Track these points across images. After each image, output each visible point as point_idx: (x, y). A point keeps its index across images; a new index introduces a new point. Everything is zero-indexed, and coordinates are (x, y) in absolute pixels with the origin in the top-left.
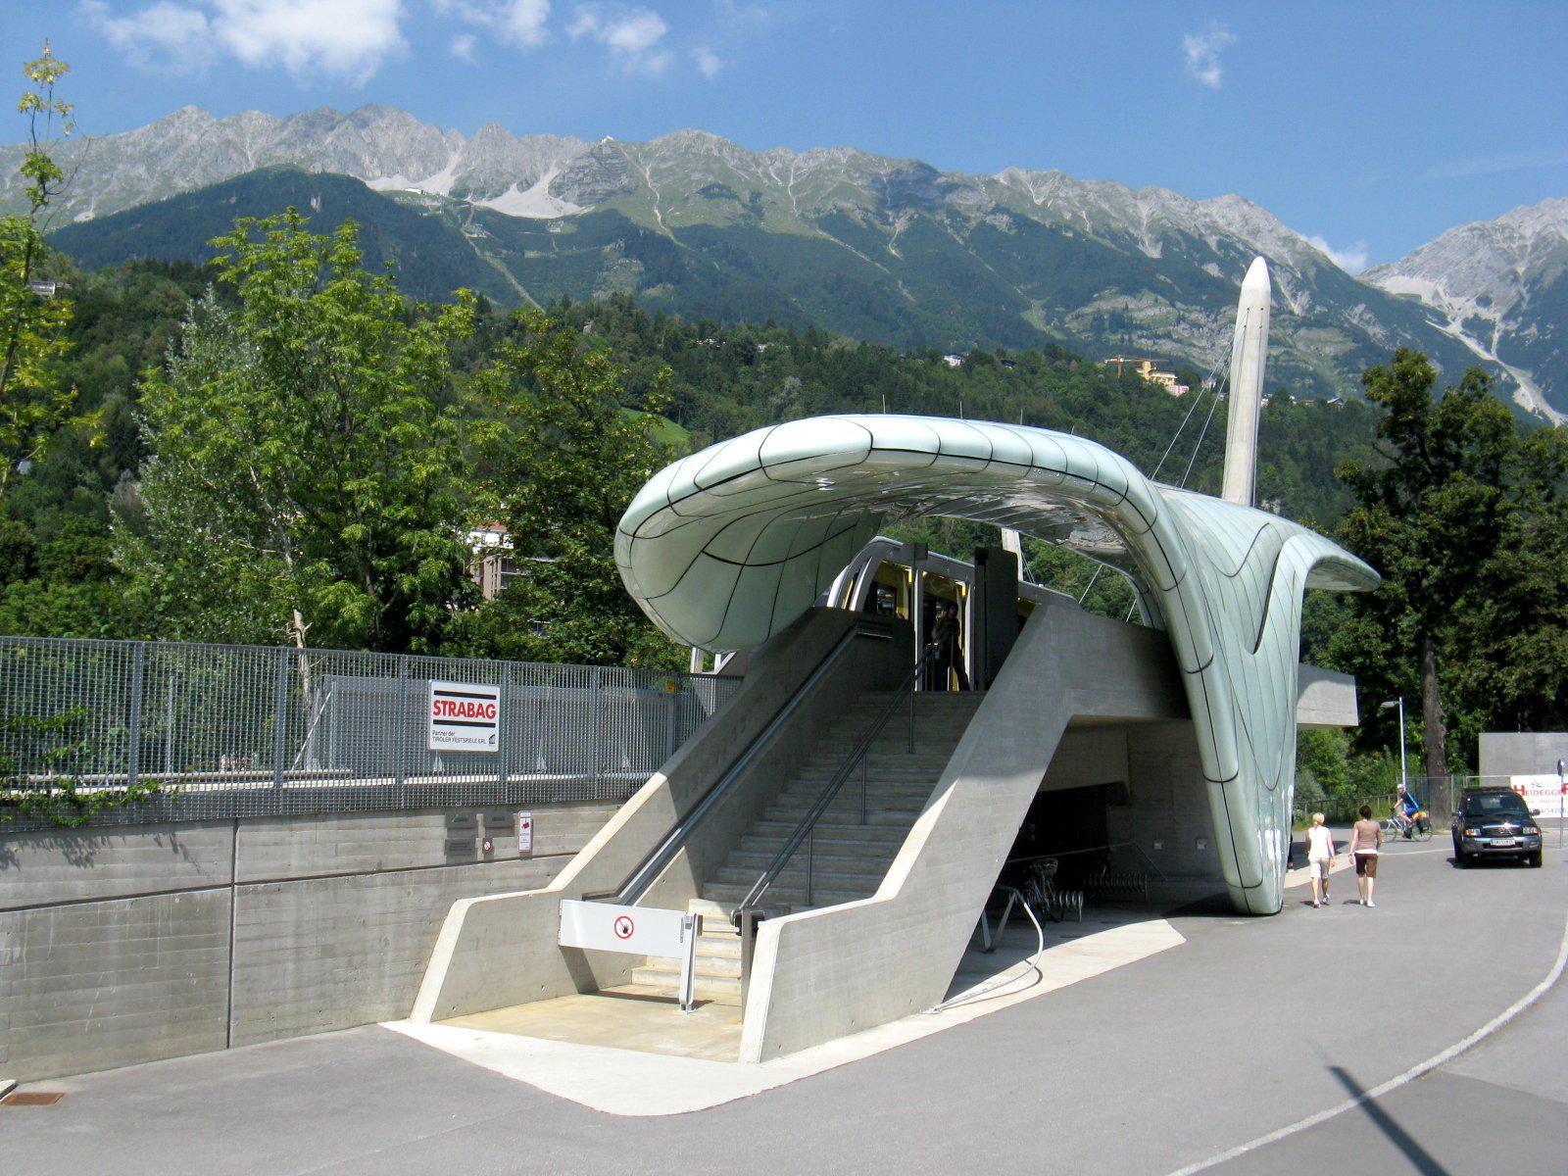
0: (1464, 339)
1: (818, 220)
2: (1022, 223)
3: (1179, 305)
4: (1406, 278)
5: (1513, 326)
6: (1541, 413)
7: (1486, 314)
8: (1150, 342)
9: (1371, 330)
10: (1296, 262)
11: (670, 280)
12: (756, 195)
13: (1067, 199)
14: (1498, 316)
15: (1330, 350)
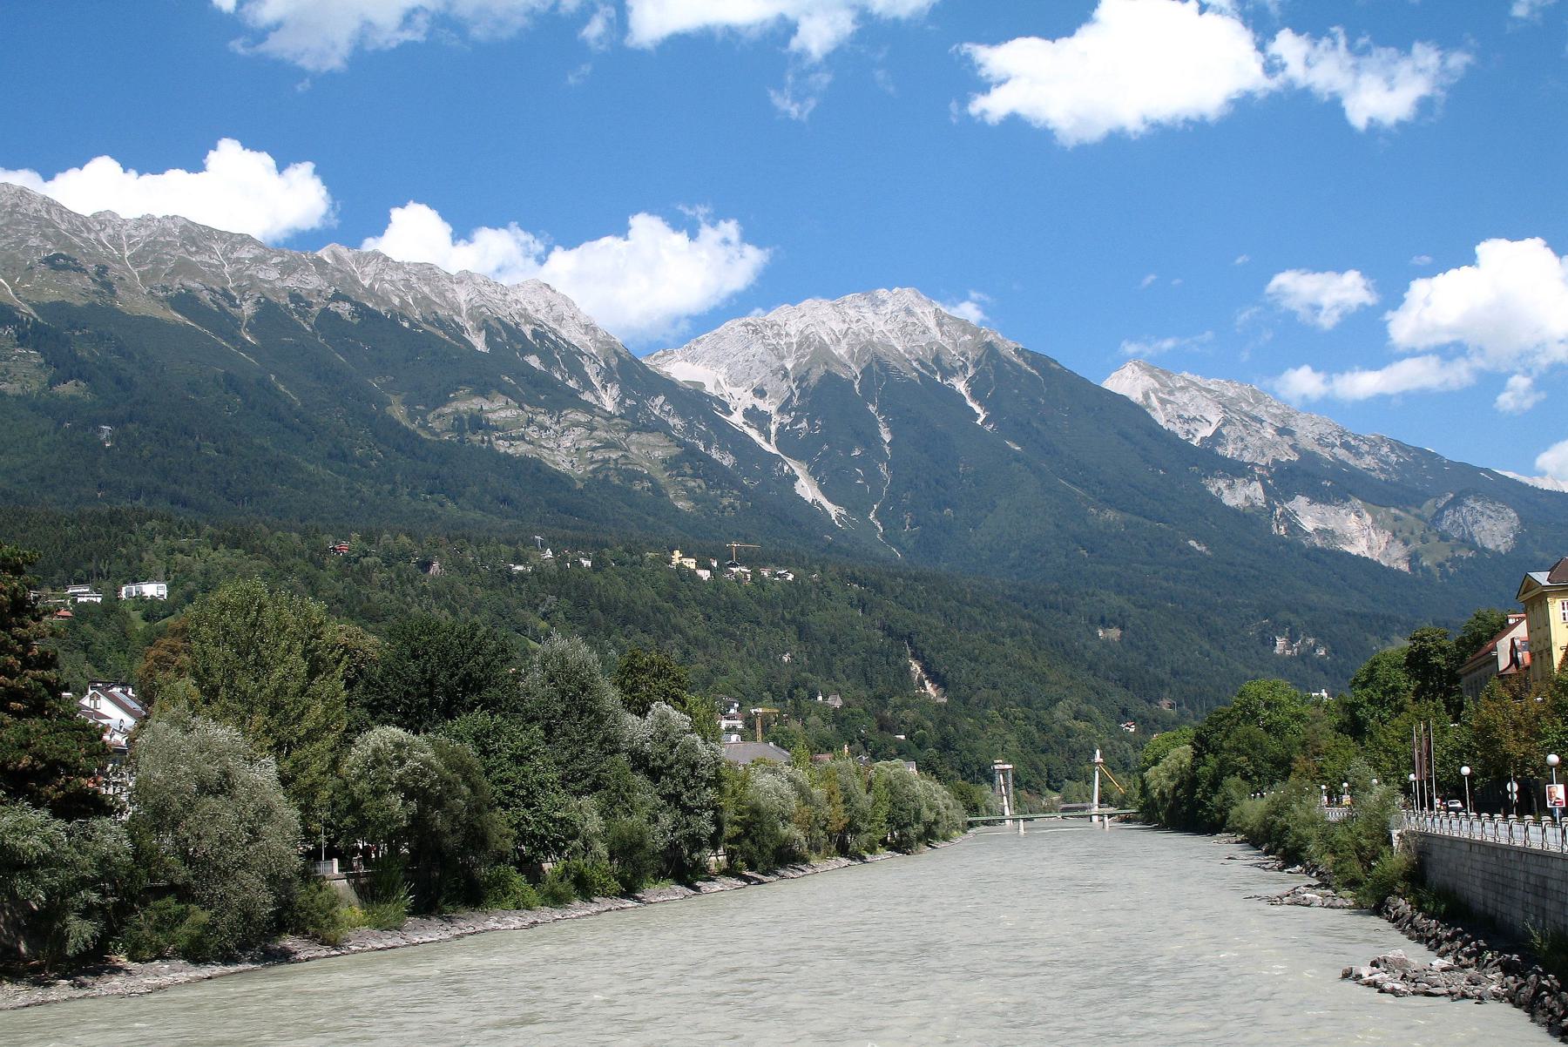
0: (746, 428)
1: (168, 299)
2: (361, 310)
3: (527, 407)
4: (689, 365)
5: (787, 420)
6: (819, 504)
7: (764, 405)
8: (507, 444)
9: (671, 421)
10: (600, 350)
11: (80, 377)
12: (102, 270)
13: (392, 282)
14: (773, 409)
15: (658, 454)
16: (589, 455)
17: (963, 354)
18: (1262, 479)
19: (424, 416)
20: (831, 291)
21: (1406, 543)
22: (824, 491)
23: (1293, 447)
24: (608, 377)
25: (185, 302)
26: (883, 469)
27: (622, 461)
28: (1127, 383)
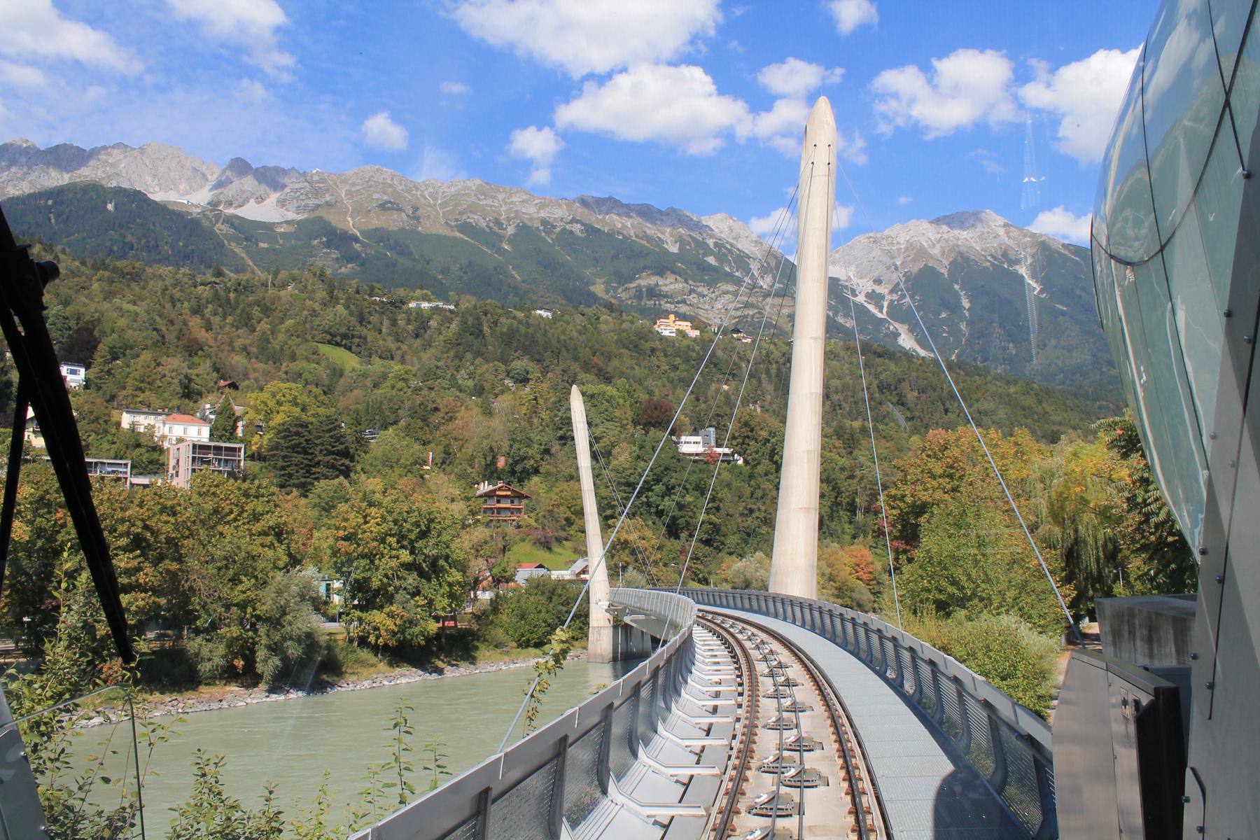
1: (457, 226)
5: (895, 297)
7: (879, 289)
24: (764, 270)
25: (466, 228)
26: (963, 326)
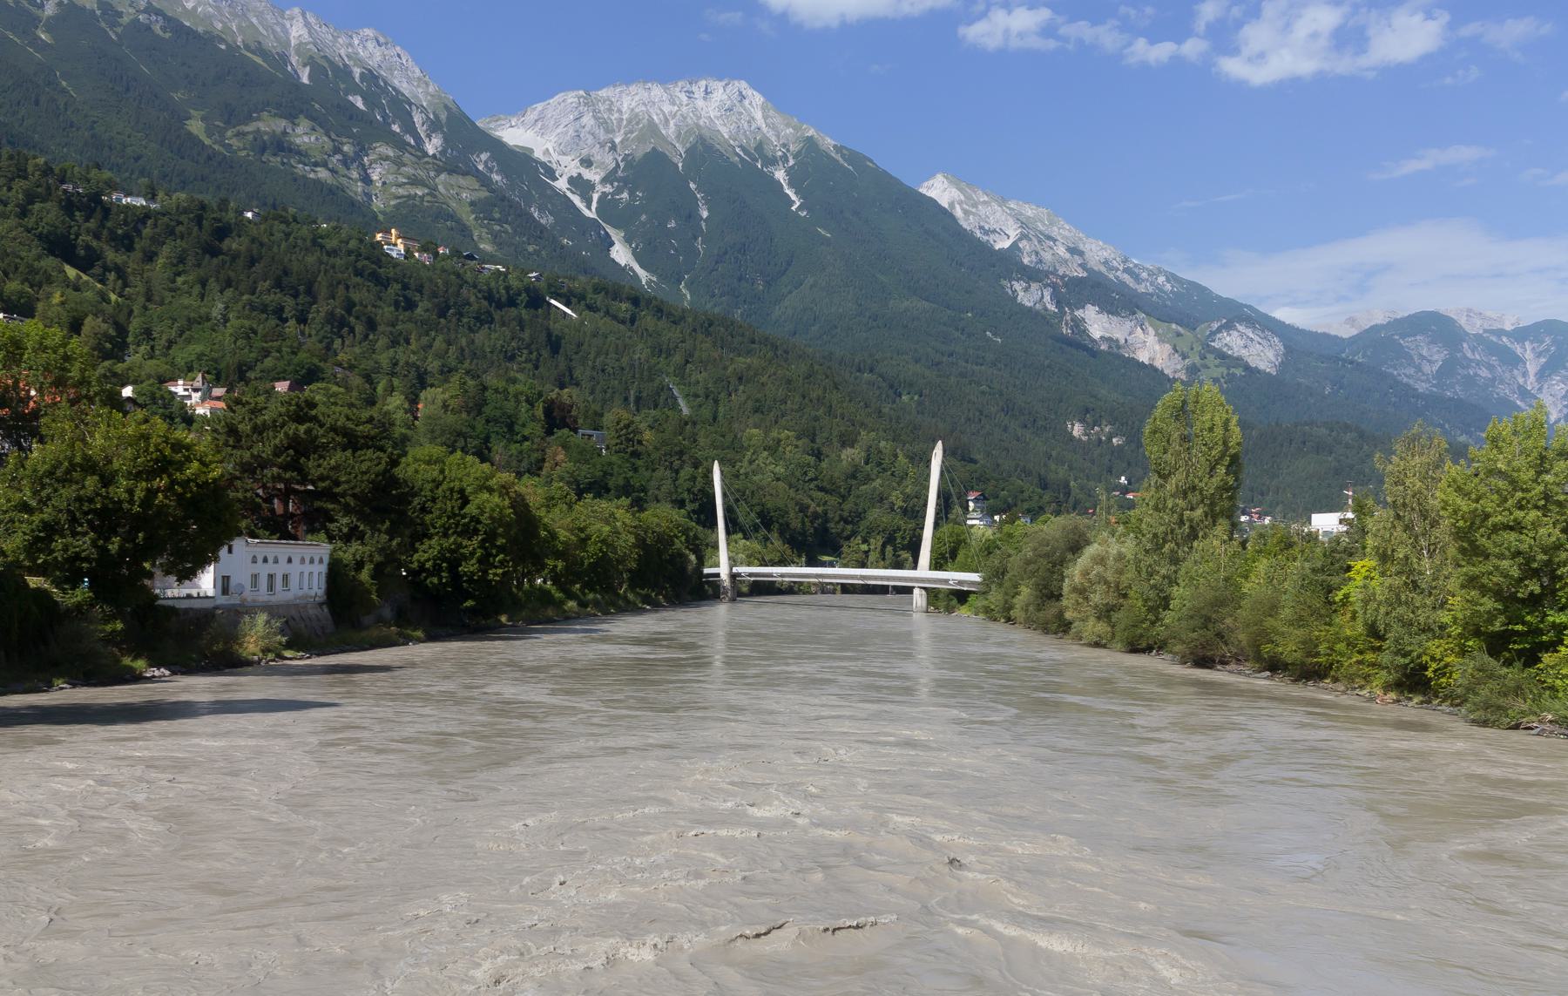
0: (569, 194)
6: (631, 269)
7: (588, 175)
10: (430, 103)
16: (393, 190)
17: (784, 145)
18: (1054, 286)
19: (222, 132)
20: (665, 78)
21: (1184, 357)
22: (637, 256)
23: (1083, 266)
24: (434, 126)
27: (428, 198)
28: (939, 190)
